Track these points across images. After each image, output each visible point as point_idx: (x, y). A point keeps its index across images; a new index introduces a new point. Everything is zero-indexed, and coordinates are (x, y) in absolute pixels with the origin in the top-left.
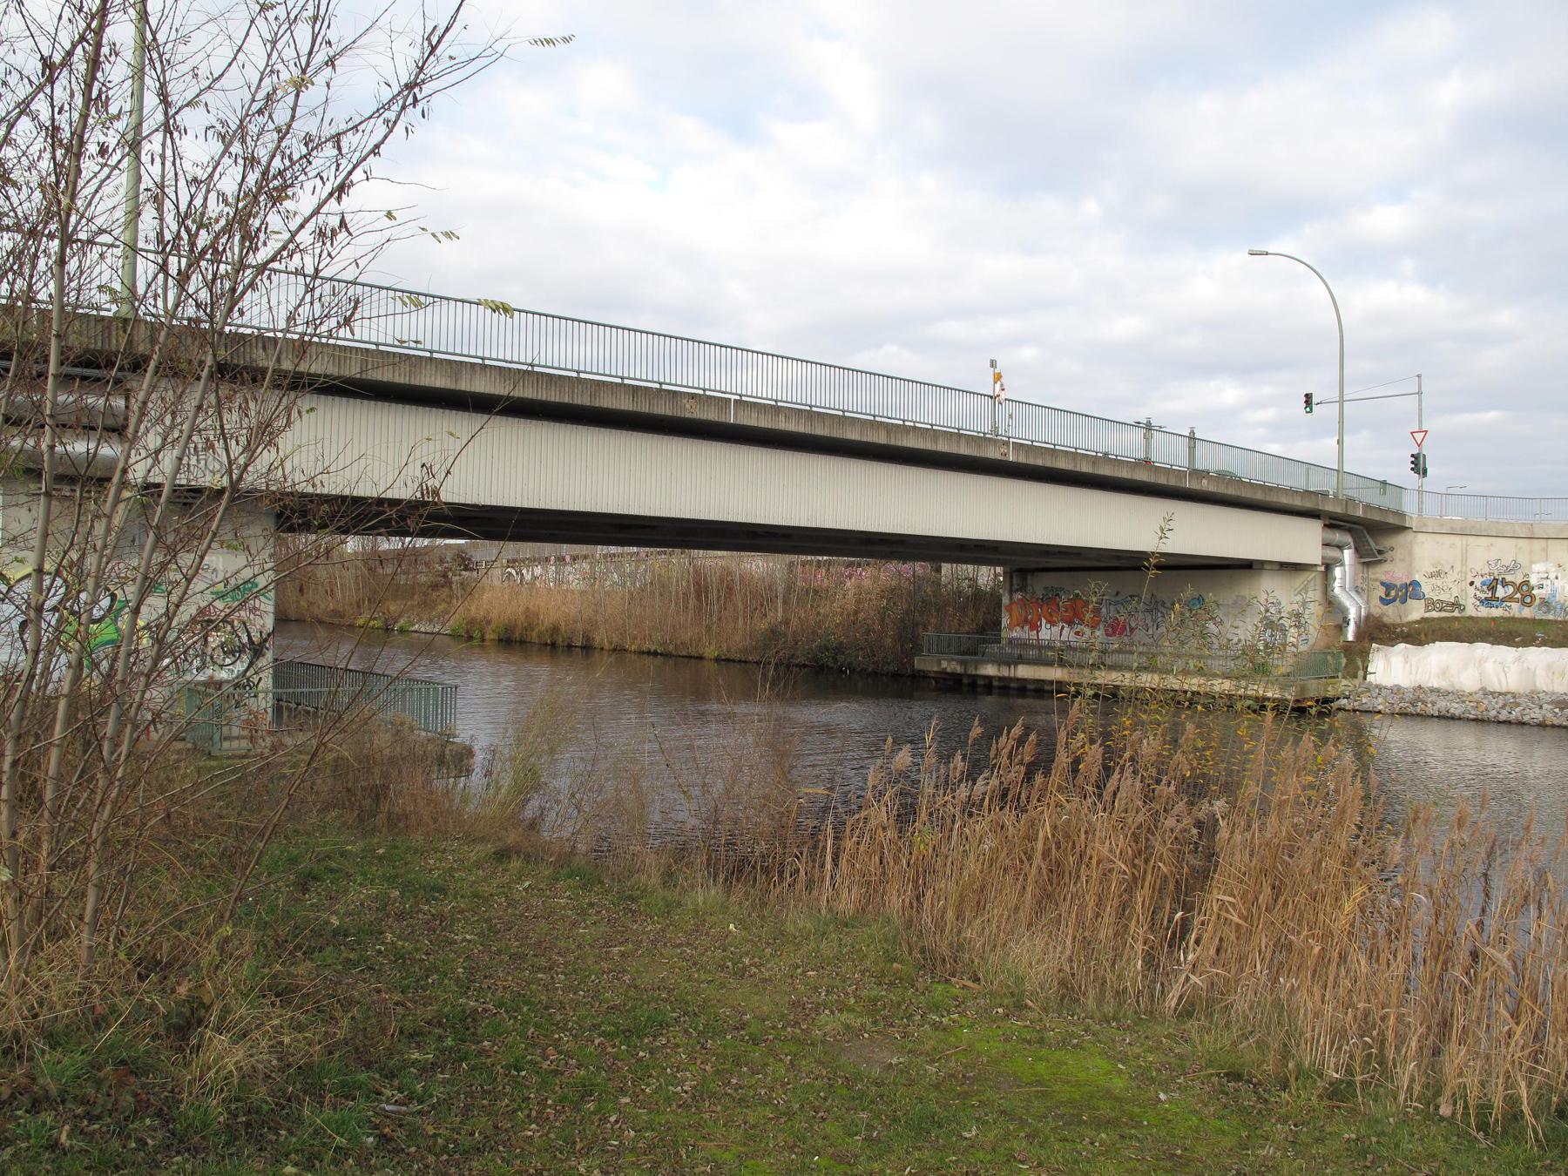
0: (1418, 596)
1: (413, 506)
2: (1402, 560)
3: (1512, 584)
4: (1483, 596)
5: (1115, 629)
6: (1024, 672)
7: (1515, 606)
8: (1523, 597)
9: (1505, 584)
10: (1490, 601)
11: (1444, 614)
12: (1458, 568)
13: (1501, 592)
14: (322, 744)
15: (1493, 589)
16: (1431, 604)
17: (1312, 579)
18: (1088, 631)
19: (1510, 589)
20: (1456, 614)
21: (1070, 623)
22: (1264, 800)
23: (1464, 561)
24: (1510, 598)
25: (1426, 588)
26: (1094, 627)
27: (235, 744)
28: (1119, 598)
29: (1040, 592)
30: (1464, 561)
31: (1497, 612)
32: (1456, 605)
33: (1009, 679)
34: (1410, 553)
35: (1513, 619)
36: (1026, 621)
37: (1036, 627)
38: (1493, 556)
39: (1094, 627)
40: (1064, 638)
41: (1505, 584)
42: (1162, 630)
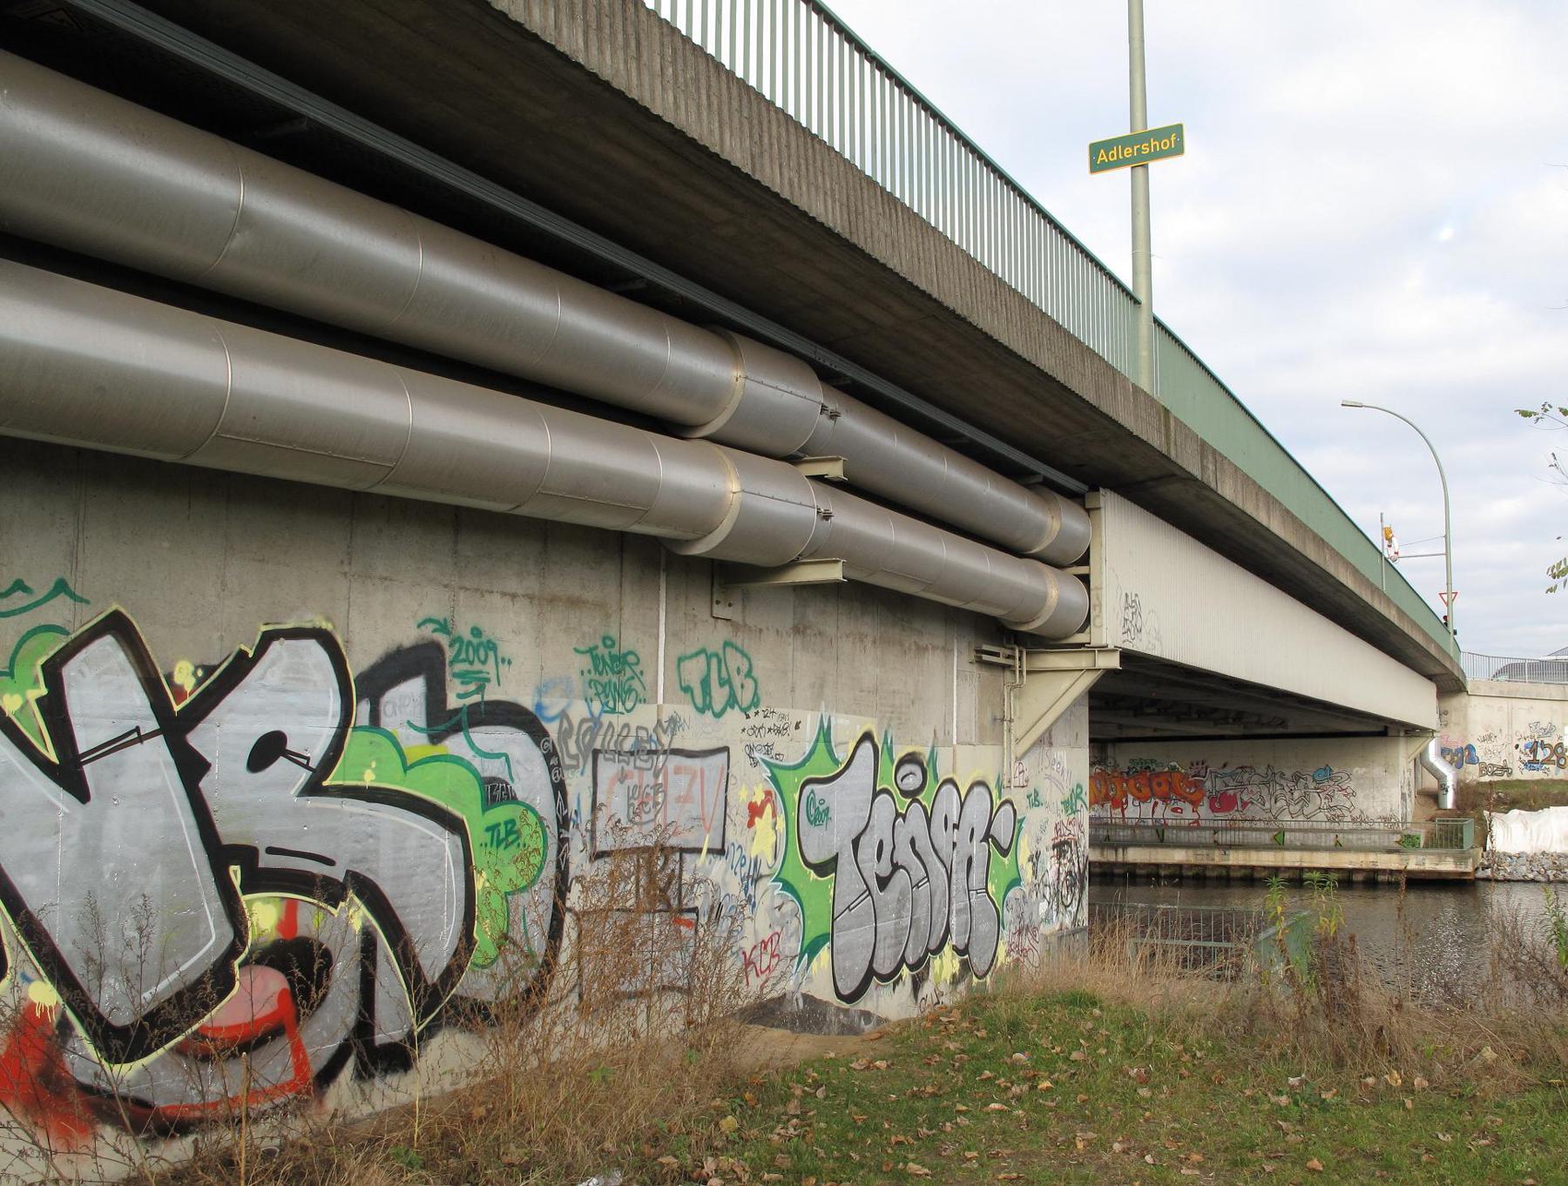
0: (1472, 761)
1: (29, 915)
2: (1458, 724)
3: (1549, 746)
4: (1526, 759)
5: (1223, 802)
6: (1135, 855)
7: (1552, 768)
8: (1559, 759)
9: (1544, 746)
10: (1532, 764)
11: (1496, 778)
12: (1505, 732)
13: (1541, 756)
14: (1218, 1150)
15: (1534, 751)
16: (1484, 769)
17: (785, 875)
18: (1187, 807)
19: (1548, 751)
20: (1505, 777)
21: (1166, 799)
22: (1438, 1010)
23: (1510, 723)
24: (1547, 761)
25: (1479, 753)
26: (1195, 804)
27: (1375, 837)
28: (1227, 770)
29: (1124, 765)
30: (1510, 723)
31: (1537, 775)
32: (1505, 769)
33: (1114, 864)
34: (1465, 717)
35: (1554, 782)
36: (1107, 798)
37: (1119, 804)
38: (1534, 718)
39: (1195, 804)
40: (1158, 814)
41: (1544, 746)
42: (1282, 803)
